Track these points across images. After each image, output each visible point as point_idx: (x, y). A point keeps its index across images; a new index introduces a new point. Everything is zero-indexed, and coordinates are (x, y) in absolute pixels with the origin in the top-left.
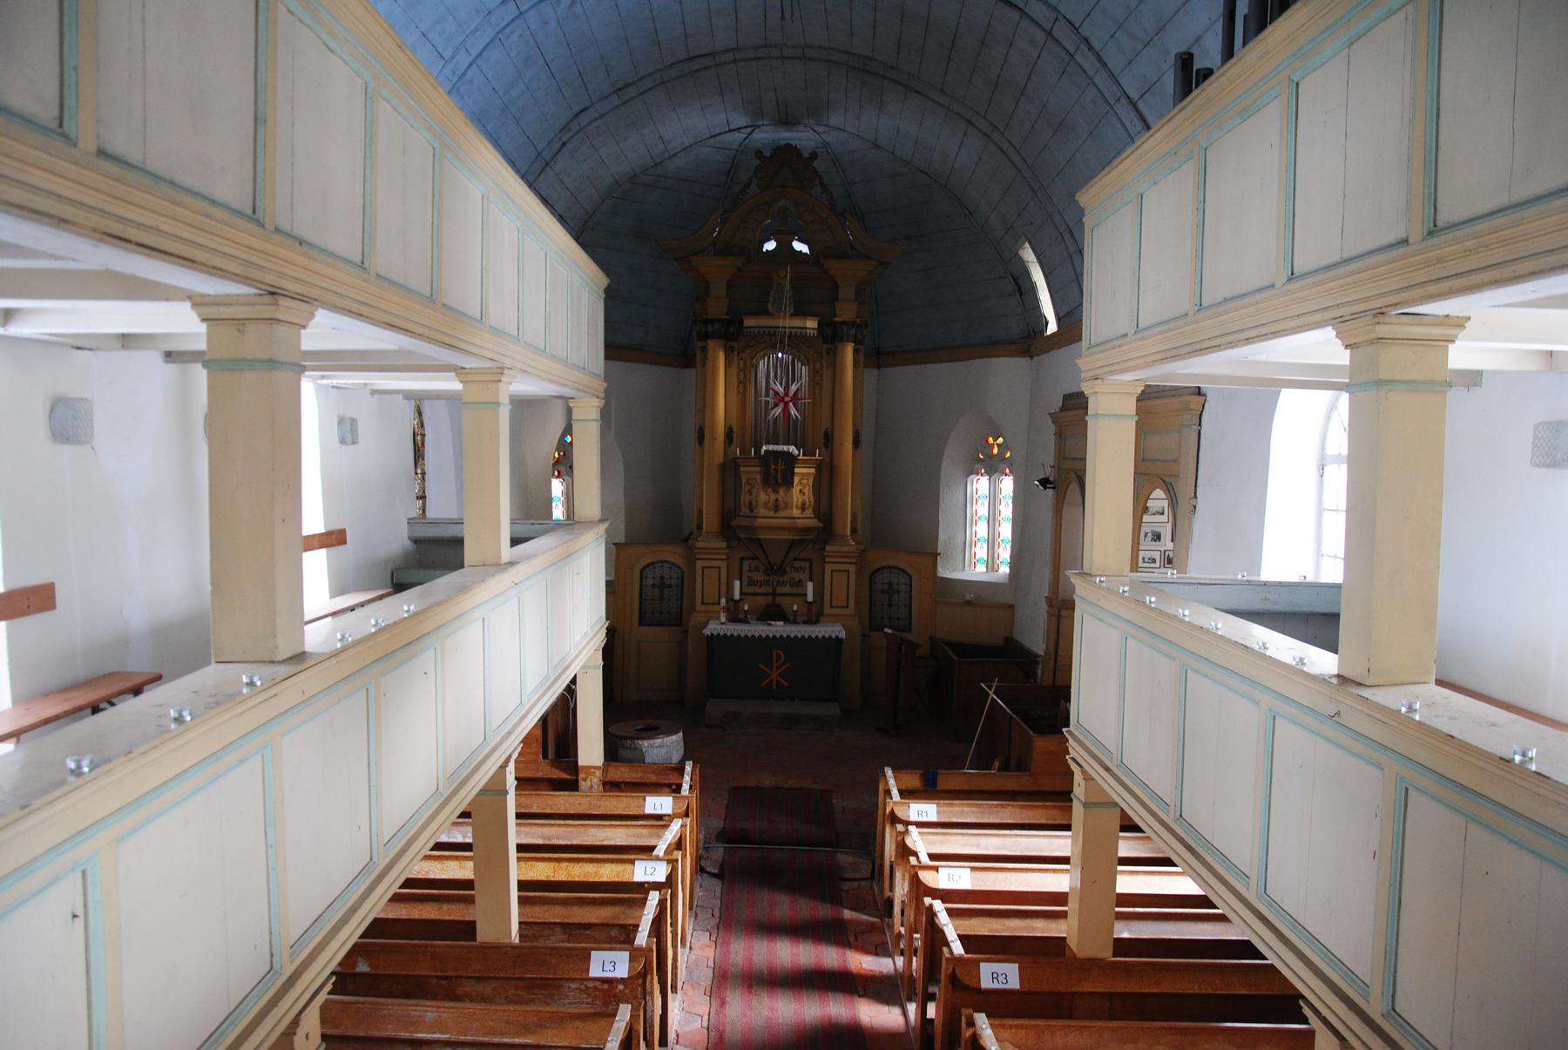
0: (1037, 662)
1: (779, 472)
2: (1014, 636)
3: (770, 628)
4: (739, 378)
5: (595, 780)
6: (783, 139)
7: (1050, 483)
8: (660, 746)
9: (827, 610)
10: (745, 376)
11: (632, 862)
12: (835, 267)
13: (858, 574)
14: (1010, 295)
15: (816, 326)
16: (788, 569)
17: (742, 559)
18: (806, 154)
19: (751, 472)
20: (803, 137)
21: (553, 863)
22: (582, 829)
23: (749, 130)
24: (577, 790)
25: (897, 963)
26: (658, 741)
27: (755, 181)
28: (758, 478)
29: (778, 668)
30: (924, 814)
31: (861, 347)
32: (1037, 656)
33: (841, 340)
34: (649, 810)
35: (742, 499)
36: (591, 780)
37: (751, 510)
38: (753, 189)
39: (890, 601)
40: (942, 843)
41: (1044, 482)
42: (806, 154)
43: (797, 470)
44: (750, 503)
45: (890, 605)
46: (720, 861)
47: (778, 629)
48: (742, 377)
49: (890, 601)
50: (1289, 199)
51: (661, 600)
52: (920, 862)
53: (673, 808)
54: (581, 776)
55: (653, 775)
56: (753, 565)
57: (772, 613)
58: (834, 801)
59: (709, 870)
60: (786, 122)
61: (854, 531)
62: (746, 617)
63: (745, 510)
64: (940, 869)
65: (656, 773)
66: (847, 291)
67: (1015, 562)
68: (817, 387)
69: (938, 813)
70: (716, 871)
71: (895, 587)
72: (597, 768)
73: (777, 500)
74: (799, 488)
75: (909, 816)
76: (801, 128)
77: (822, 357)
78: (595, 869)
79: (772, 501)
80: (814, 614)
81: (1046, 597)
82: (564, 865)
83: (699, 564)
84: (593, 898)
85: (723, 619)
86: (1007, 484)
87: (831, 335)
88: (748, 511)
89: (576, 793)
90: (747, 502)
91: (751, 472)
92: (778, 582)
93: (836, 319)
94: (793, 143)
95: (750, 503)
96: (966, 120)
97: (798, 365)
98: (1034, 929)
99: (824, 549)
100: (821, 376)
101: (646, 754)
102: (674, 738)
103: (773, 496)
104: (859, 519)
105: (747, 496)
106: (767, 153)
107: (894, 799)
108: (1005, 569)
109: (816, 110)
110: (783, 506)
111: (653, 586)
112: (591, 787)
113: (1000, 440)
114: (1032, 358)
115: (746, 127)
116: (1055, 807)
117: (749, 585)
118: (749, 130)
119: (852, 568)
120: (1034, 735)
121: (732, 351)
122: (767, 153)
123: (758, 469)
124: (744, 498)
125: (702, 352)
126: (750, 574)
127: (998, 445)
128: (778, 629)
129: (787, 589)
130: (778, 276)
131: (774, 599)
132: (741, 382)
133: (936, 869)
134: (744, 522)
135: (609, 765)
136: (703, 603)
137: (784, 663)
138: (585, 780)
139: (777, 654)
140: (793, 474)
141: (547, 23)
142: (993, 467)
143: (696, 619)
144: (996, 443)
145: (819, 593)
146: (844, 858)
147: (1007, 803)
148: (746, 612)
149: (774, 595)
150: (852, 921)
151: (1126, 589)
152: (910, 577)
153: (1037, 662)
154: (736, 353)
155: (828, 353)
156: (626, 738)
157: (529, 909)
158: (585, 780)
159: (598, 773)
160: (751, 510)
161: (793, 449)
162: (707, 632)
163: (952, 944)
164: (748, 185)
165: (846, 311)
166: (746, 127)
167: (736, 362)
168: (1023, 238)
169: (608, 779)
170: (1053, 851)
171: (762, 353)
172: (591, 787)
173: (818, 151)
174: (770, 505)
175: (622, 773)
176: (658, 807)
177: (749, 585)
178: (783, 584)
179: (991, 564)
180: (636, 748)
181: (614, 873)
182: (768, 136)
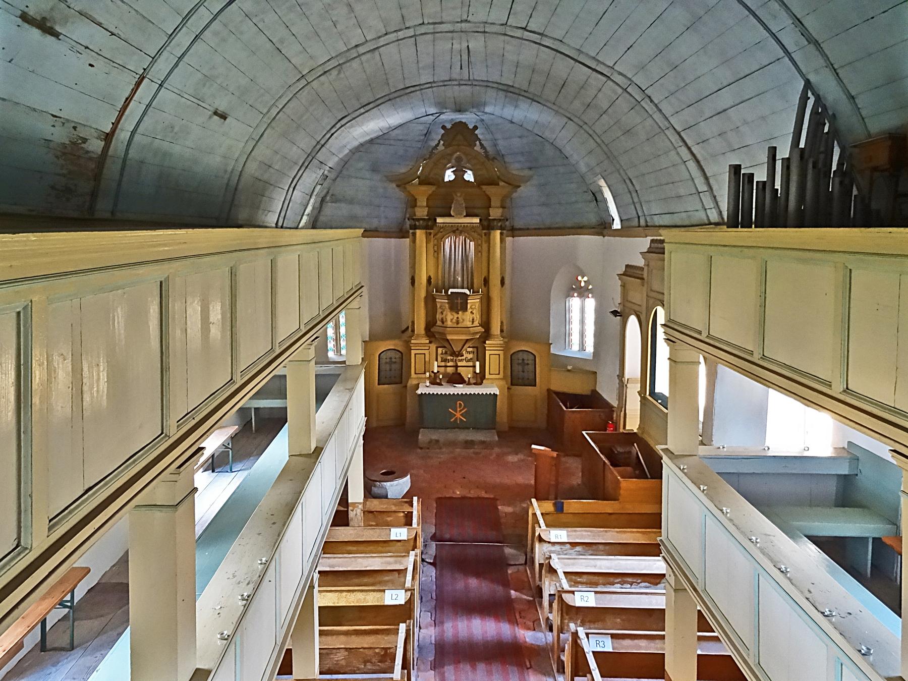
0: (613, 411)
1: (459, 304)
2: (597, 389)
3: (455, 389)
4: (434, 250)
5: (359, 511)
6: (458, 118)
7: (619, 313)
8: (397, 485)
9: (487, 376)
10: (438, 248)
11: (384, 591)
12: (489, 190)
13: (505, 354)
14: (590, 202)
15: (478, 222)
16: (464, 352)
17: (437, 348)
18: (471, 127)
19: (442, 302)
20: (469, 118)
21: (337, 593)
22: (353, 559)
23: (438, 115)
24: (347, 525)
25: (548, 638)
26: (395, 483)
27: (442, 142)
28: (447, 306)
29: (460, 411)
30: (559, 537)
31: (505, 231)
32: (613, 407)
33: (493, 229)
34: (393, 537)
35: (437, 316)
36: (356, 511)
37: (443, 323)
38: (441, 147)
39: (523, 369)
40: (573, 564)
41: (615, 313)
42: (471, 127)
43: (469, 301)
44: (442, 319)
45: (523, 372)
46: (434, 555)
47: (460, 389)
48: (436, 249)
49: (523, 369)
50: (844, 341)
51: (390, 370)
52: (563, 588)
53: (408, 536)
54: (350, 508)
55: (393, 506)
56: (444, 351)
57: (456, 379)
58: (499, 507)
59: (427, 560)
60: (459, 111)
61: (502, 331)
62: (441, 382)
63: (439, 323)
64: (575, 593)
65: (395, 505)
66: (495, 202)
67: (597, 345)
68: (480, 253)
69: (568, 536)
70: (432, 561)
71: (526, 362)
72: (360, 503)
73: (458, 318)
74: (470, 310)
75: (550, 539)
76: (467, 113)
77: (482, 237)
78: (363, 597)
79: (455, 318)
80: (480, 379)
81: (618, 376)
82: (344, 594)
83: (413, 352)
84: (365, 630)
85: (428, 384)
86: (590, 303)
87: (488, 225)
88: (441, 323)
89: (348, 528)
90: (440, 319)
91: (442, 302)
92: (430, 234)
93: (490, 218)
94: (464, 121)
95: (442, 319)
96: (567, 117)
97: (468, 241)
98: (640, 648)
99: (485, 343)
100: (482, 247)
101: (388, 491)
102: (405, 479)
103: (456, 316)
104: (505, 323)
105: (441, 314)
106: (449, 126)
107: (542, 528)
108: (590, 348)
109: (477, 105)
110: (462, 320)
111: (386, 363)
112: (356, 514)
113: (586, 279)
114: (604, 237)
115: (436, 113)
116: (638, 532)
117: (442, 361)
118: (438, 115)
119: (501, 353)
120: (621, 480)
121: (430, 235)
122: (449, 126)
123: (447, 301)
124: (439, 316)
125: (413, 235)
126: (442, 356)
127: (585, 281)
128: (460, 389)
129: (464, 363)
130: (456, 195)
131: (457, 369)
132: (435, 252)
133: (573, 592)
134: (441, 330)
135: (367, 501)
136: (415, 374)
137: (463, 409)
138: (352, 511)
139: (460, 403)
140: (467, 303)
141: (324, 84)
142: (583, 292)
143: (412, 382)
144: (583, 280)
145: (483, 367)
146: (508, 551)
147: (609, 529)
148: (441, 379)
149: (456, 367)
150: (518, 600)
151: (705, 488)
152: (535, 356)
153: (613, 411)
154: (432, 236)
155: (485, 235)
156: (376, 481)
157: (324, 638)
158: (352, 511)
159: (361, 506)
160: (443, 323)
161: (467, 292)
162: (419, 392)
163: (593, 672)
164: (438, 145)
165: (495, 213)
166: (436, 113)
167: (432, 239)
168: (600, 176)
169: (366, 510)
170: (642, 570)
171: (448, 235)
172: (356, 514)
173: (477, 124)
174: (454, 321)
175: (375, 504)
176: (398, 535)
177: (442, 361)
178: (461, 360)
179: (582, 348)
180: (382, 487)
181: (376, 599)
182: (449, 117)
